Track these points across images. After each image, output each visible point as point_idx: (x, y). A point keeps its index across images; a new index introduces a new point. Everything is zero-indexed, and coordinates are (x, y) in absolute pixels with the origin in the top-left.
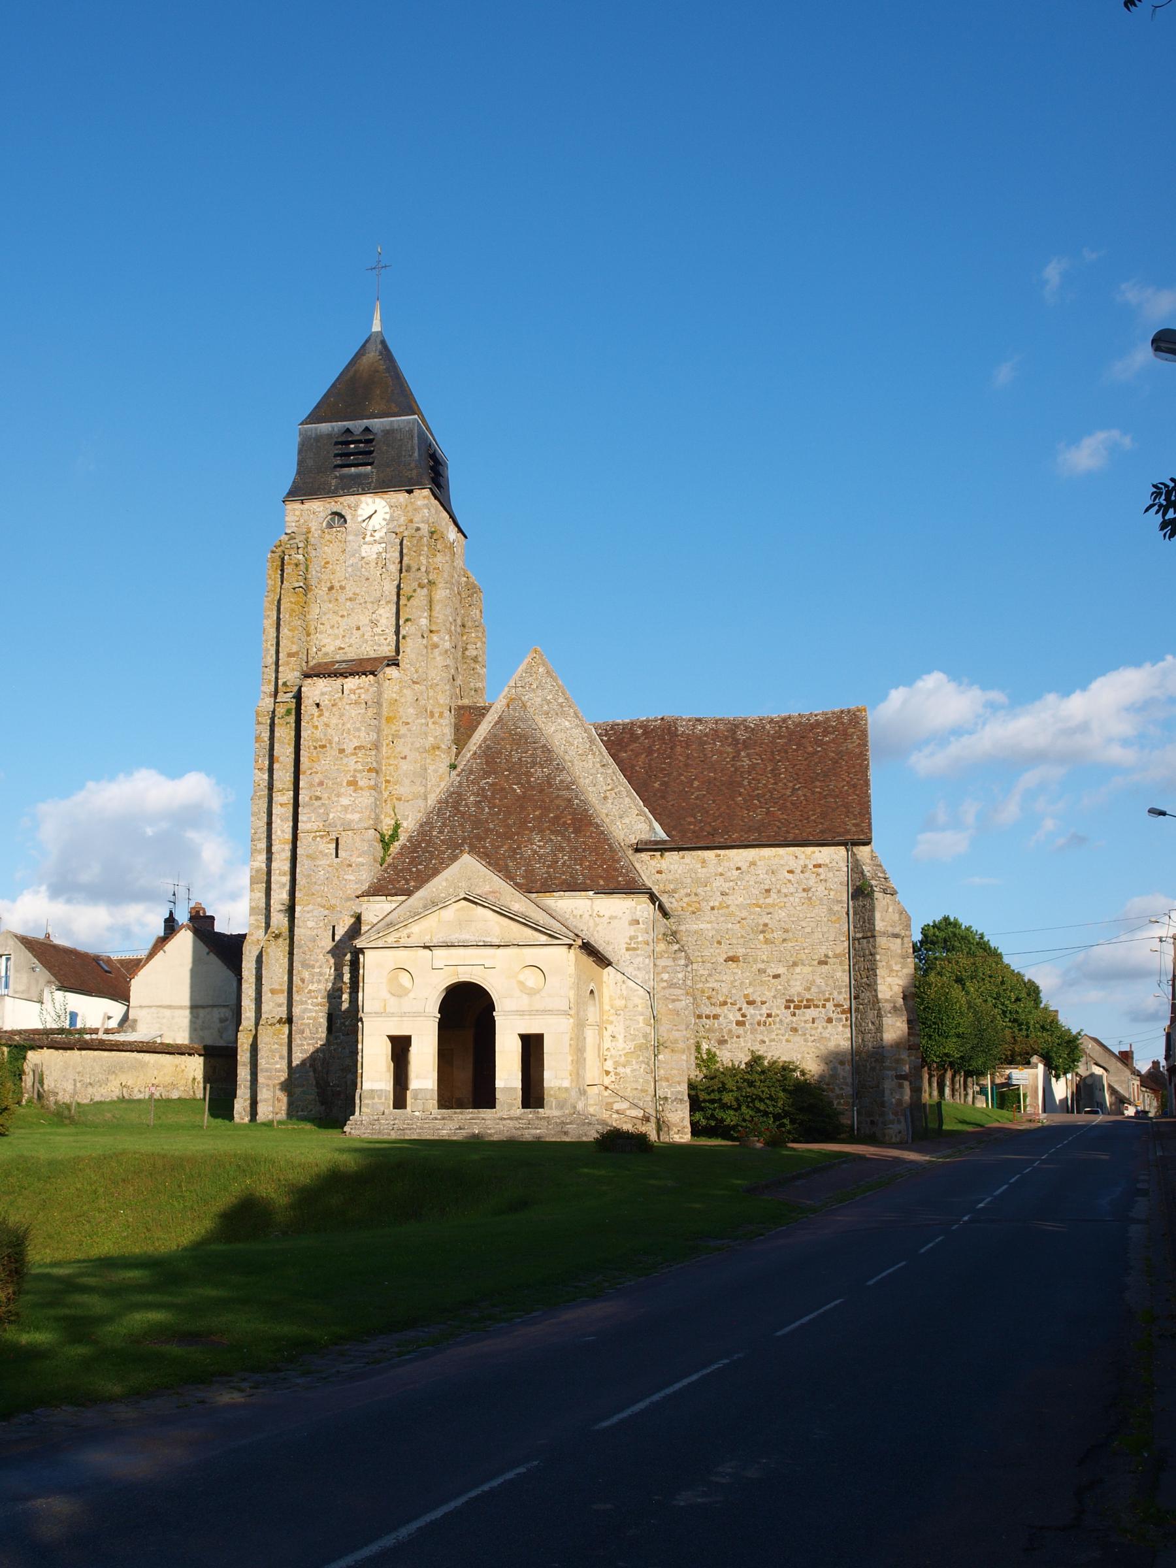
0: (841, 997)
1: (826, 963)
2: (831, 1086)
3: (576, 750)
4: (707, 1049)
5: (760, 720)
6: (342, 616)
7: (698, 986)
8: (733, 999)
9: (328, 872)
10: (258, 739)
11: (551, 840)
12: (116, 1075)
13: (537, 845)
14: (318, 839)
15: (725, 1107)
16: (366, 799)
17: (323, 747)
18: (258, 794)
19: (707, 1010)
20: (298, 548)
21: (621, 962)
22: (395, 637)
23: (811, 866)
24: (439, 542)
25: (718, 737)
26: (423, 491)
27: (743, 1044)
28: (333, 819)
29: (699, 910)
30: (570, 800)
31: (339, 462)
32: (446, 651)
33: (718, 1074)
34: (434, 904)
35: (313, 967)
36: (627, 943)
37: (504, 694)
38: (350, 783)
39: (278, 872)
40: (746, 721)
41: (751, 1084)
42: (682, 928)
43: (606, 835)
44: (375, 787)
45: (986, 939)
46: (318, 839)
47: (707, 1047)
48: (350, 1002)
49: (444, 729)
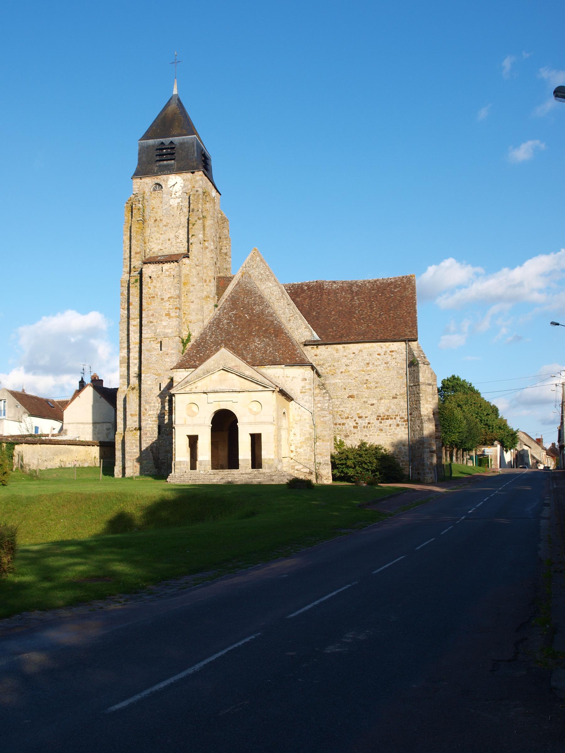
0: (403, 414)
1: (396, 398)
2: (399, 457)
3: (275, 297)
4: (339, 440)
5: (364, 281)
6: (161, 234)
7: (335, 410)
8: (352, 415)
9: (157, 358)
10: (122, 294)
11: (264, 341)
12: (58, 456)
13: (257, 343)
14: (152, 342)
15: (348, 467)
16: (174, 322)
17: (153, 297)
18: (123, 321)
19: (339, 421)
20: (139, 201)
21: (298, 398)
22: (187, 244)
23: (388, 352)
24: (207, 197)
25: (344, 290)
26: (199, 172)
27: (357, 437)
28: (159, 332)
29: (335, 373)
30: (272, 321)
31: (158, 159)
32: (212, 250)
33: (345, 451)
34: (208, 372)
35: (151, 403)
36: (301, 390)
37: (240, 270)
38: (167, 315)
39: (133, 358)
40: (357, 282)
41: (361, 456)
42: (327, 382)
43: (290, 338)
44: (178, 317)
45: (472, 386)
46: (152, 342)
47: (340, 439)
48: (169, 419)
49: (212, 288)
